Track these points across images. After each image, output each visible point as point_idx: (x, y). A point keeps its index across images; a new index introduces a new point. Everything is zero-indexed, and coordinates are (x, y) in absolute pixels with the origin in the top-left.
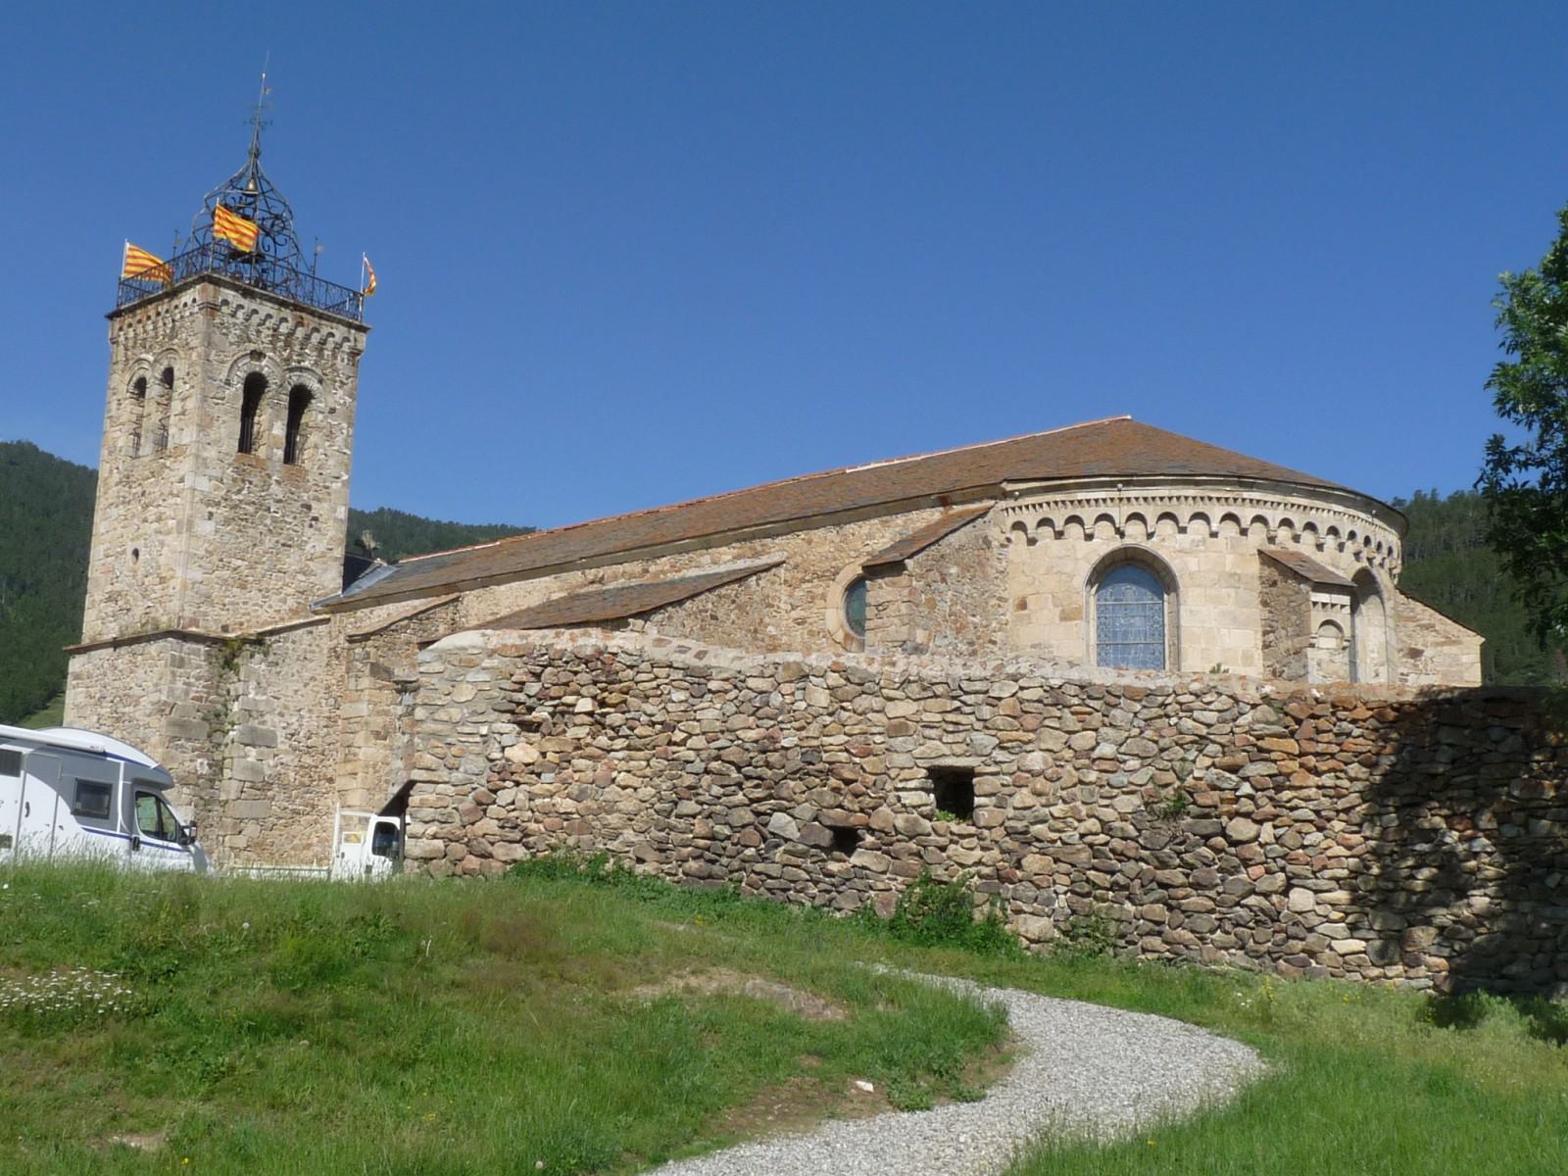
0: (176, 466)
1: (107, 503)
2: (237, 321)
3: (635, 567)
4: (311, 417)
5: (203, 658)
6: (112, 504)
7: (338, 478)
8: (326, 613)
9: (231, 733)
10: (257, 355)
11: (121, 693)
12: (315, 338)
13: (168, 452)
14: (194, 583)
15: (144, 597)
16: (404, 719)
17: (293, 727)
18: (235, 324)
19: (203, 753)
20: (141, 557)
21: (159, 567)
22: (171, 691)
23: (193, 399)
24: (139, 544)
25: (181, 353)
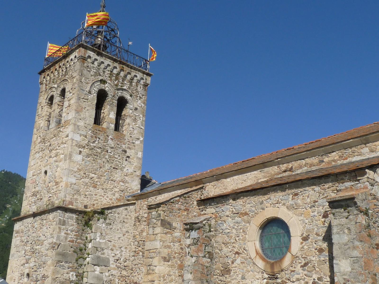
0: (65, 130)
1: (35, 152)
2: (95, 66)
3: (314, 160)
4: (127, 111)
5: (74, 221)
6: (37, 152)
7: (138, 139)
8: (133, 200)
9: (87, 259)
10: (103, 82)
11: (36, 239)
12: (129, 77)
13: (61, 125)
14: (71, 184)
15: (48, 193)
16: (193, 247)
17: (117, 256)
18: (93, 67)
19: (73, 269)
20: (48, 174)
21: (55, 178)
22: (58, 237)
23: (74, 99)
24: (47, 168)
25: (69, 81)
